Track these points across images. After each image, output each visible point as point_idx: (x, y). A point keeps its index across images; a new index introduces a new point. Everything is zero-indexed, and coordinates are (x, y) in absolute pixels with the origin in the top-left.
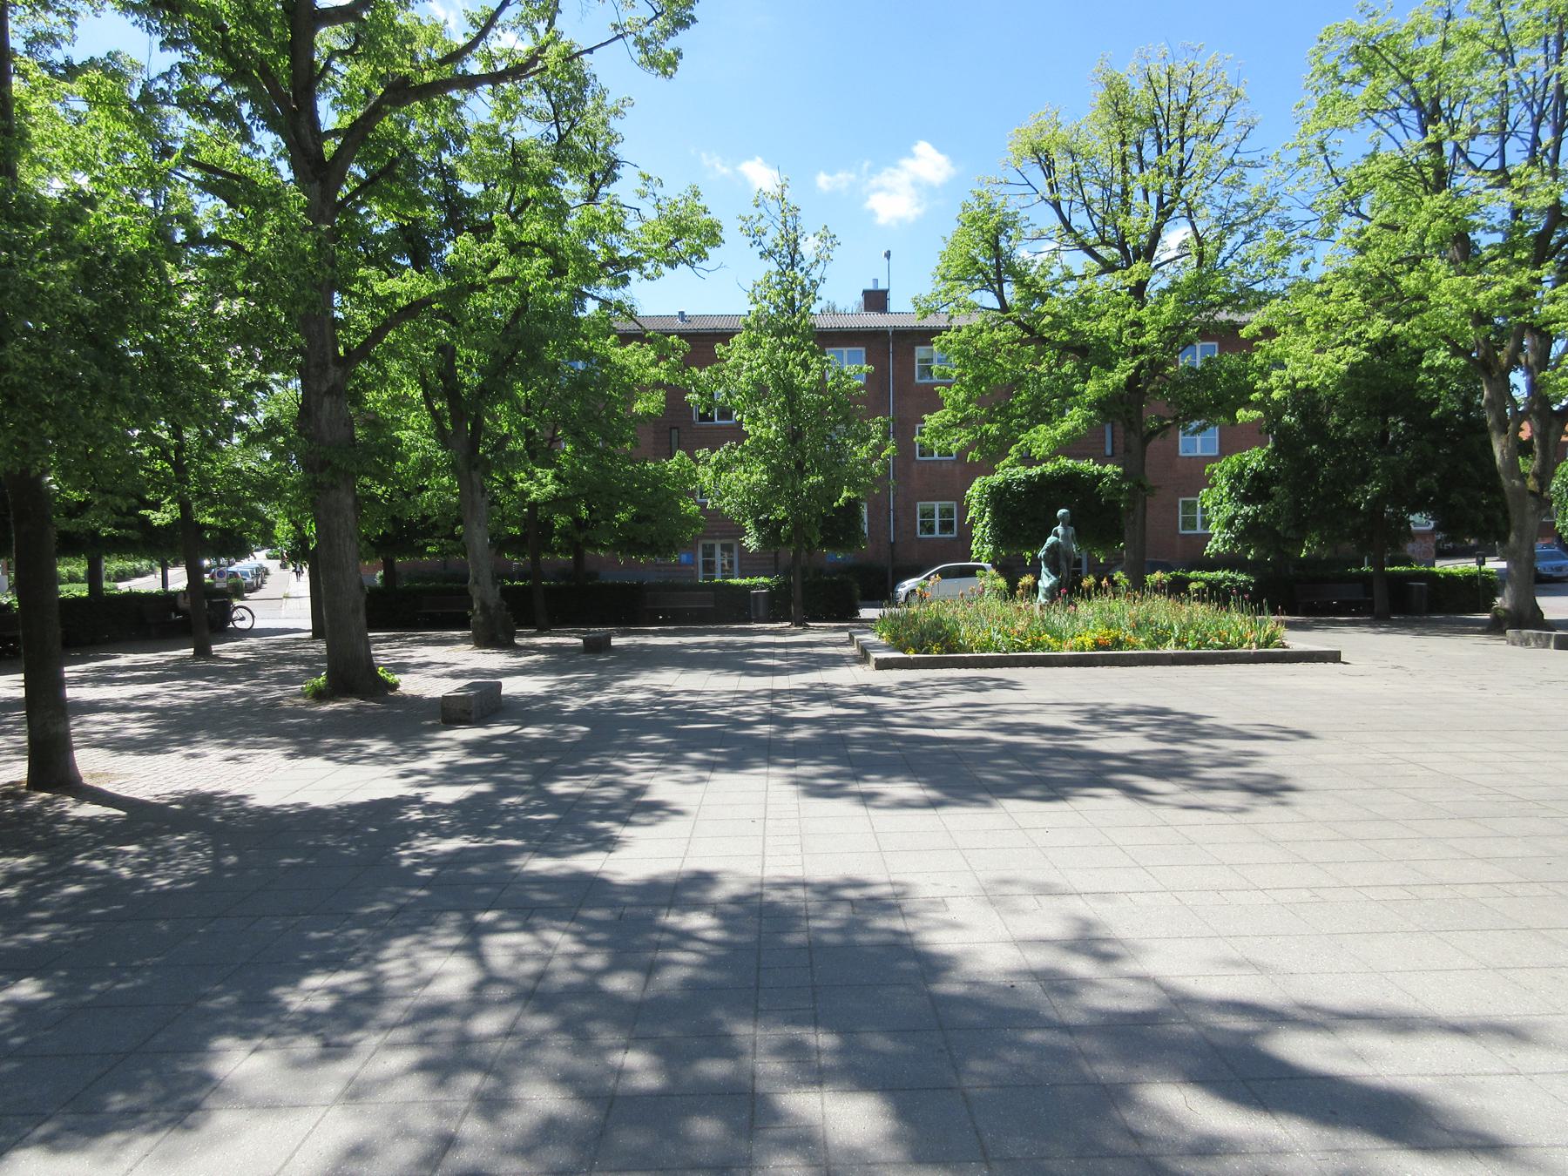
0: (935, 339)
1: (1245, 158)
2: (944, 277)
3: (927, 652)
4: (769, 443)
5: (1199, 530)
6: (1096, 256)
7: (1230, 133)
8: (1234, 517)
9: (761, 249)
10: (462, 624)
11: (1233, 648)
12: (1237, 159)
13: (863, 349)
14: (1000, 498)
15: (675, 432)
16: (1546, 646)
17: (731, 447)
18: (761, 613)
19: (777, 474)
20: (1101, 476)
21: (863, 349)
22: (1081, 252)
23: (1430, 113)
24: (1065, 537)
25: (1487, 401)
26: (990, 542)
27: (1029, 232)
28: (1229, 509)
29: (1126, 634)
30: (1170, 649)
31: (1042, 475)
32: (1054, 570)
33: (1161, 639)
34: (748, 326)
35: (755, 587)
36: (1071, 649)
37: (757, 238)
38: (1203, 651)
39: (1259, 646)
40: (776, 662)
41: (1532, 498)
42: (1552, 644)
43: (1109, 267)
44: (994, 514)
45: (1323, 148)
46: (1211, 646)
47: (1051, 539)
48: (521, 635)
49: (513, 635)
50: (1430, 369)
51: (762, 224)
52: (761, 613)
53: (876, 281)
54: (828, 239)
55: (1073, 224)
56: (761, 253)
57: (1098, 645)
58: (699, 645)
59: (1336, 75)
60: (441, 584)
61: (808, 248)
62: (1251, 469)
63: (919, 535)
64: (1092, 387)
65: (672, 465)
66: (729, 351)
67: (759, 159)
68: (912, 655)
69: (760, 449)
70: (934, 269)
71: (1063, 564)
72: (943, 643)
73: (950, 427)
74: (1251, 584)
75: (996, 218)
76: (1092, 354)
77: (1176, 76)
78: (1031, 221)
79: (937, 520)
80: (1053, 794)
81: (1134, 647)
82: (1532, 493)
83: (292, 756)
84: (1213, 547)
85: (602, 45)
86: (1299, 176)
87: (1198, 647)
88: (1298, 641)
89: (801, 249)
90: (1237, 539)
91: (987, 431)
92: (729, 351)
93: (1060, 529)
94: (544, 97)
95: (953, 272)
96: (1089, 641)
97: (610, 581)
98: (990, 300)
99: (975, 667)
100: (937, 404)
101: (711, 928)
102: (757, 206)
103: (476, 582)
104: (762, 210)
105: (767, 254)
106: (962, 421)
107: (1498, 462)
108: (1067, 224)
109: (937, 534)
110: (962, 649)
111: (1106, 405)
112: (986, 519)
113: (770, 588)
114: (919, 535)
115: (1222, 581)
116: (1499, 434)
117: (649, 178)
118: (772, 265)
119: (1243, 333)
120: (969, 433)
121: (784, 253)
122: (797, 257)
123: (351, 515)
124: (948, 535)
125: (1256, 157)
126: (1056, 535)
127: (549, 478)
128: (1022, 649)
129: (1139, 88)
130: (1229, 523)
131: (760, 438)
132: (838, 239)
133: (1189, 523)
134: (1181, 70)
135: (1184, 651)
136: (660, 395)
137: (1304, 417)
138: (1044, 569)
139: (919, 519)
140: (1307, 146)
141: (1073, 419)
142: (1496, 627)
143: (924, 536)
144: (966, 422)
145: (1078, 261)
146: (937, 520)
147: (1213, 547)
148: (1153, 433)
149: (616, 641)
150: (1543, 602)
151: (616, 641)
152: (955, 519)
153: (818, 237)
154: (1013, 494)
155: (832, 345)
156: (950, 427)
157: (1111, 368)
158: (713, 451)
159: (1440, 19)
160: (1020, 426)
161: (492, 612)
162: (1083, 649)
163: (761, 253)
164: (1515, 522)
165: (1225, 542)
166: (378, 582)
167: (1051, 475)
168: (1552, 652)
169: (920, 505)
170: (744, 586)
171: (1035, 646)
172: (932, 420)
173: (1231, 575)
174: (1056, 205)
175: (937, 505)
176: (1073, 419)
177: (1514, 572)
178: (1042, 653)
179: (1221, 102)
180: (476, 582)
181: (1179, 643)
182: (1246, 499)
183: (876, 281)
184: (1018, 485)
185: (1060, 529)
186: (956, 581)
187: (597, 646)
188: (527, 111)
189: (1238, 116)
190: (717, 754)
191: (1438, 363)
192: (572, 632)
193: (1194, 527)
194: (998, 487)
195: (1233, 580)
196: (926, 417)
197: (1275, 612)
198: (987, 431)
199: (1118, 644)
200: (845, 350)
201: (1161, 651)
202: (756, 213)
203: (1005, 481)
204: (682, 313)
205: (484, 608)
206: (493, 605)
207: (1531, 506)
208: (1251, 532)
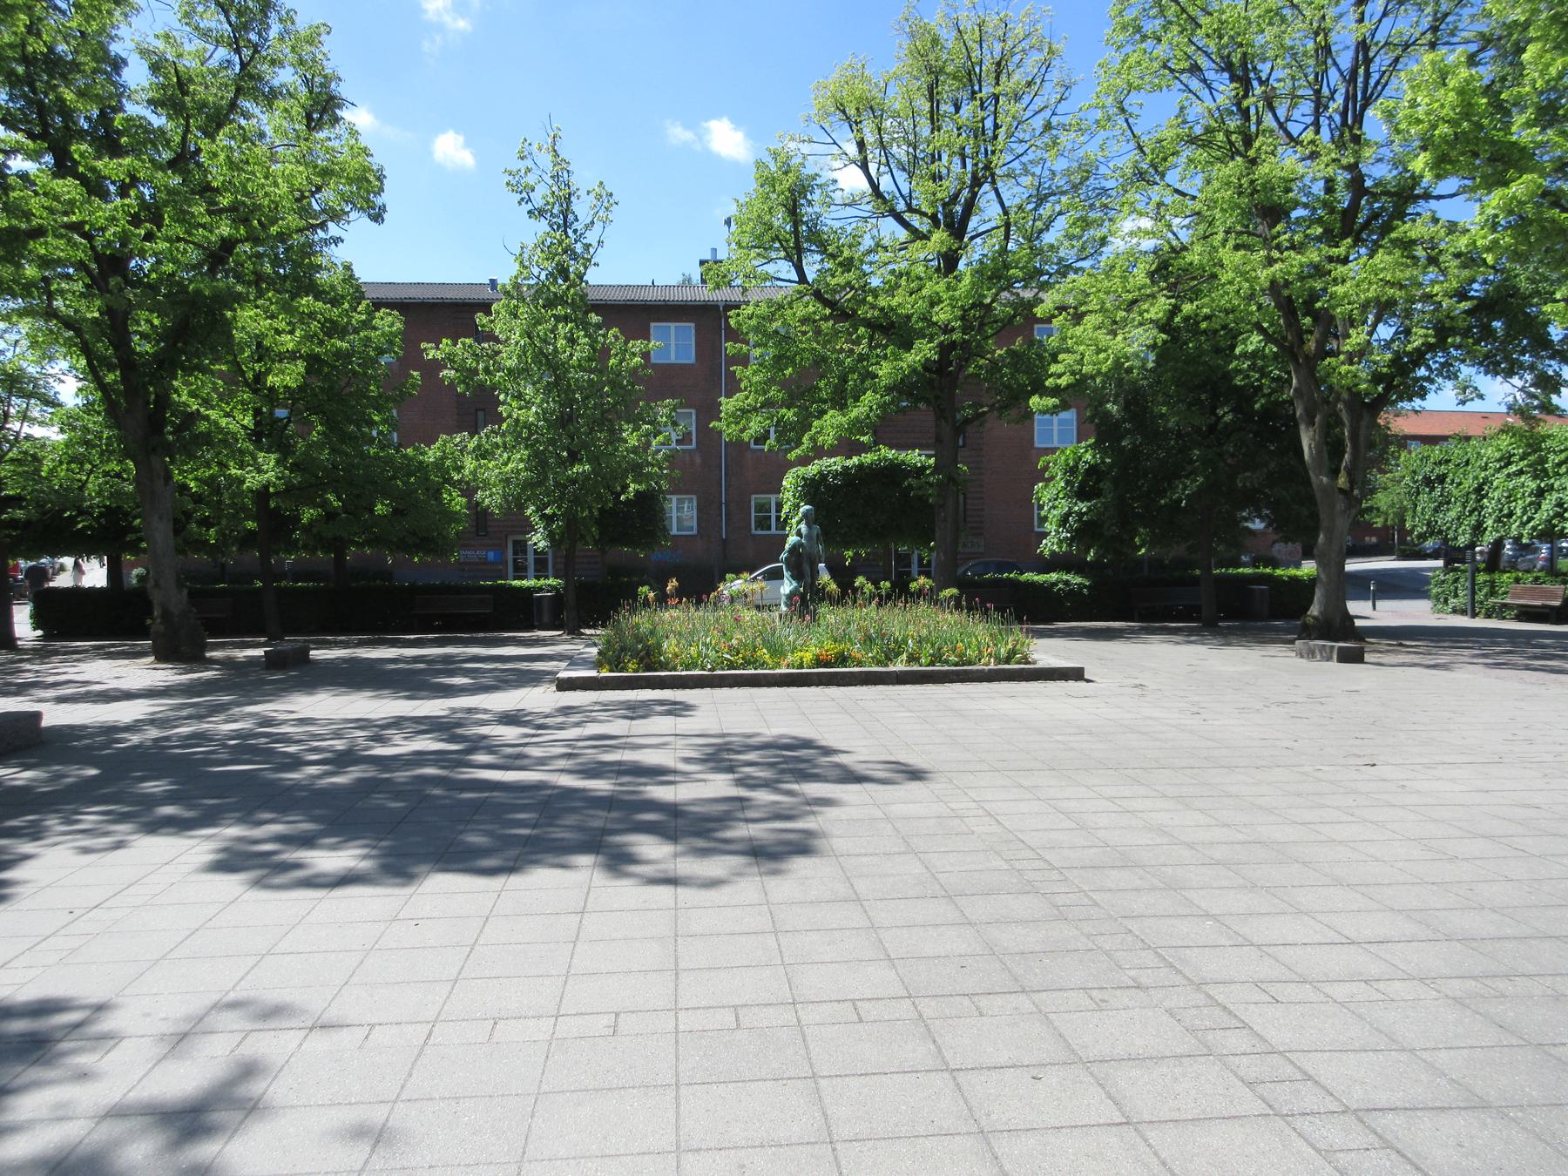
1: (1063, 120)
2: (739, 244)
5: (773, 530)
6: (906, 225)
7: (1049, 94)
8: (1069, 514)
9: (529, 206)
10: (140, 632)
11: (970, 663)
12: (1054, 121)
13: (693, 325)
14: (813, 490)
15: (481, 414)
16: (1329, 659)
18: (546, 618)
19: (539, 461)
21: (693, 325)
22: (891, 218)
23: (1241, 73)
24: (809, 537)
25: (1295, 390)
28: (1064, 506)
29: (856, 650)
30: (899, 666)
31: (860, 467)
33: (890, 656)
34: (507, 293)
35: (540, 589)
36: (788, 666)
37: (524, 195)
41: (1341, 497)
42: (1335, 657)
43: (917, 235)
46: (947, 662)
49: (205, 647)
50: (1244, 355)
51: (531, 179)
52: (546, 618)
53: (714, 251)
54: (605, 199)
56: (529, 212)
57: (819, 662)
58: (416, 659)
59: (1138, 29)
61: (582, 209)
62: (1086, 462)
63: (754, 531)
64: (884, 370)
65: (431, 454)
66: (492, 321)
67: (725, 120)
68: (605, 674)
69: (522, 434)
72: (641, 660)
74: (1085, 587)
75: (791, 178)
76: (895, 331)
81: (860, 664)
82: (1341, 490)
84: (1049, 546)
86: (1098, 140)
87: (932, 663)
89: (574, 207)
90: (1072, 539)
91: (783, 416)
92: (492, 321)
94: (222, 18)
95: (746, 240)
96: (808, 657)
98: (786, 270)
99: (662, 688)
100: (733, 388)
102: (522, 158)
103: (157, 585)
104: (528, 163)
105: (533, 213)
107: (1306, 457)
108: (875, 187)
109: (773, 530)
110: (664, 666)
111: (903, 387)
114: (754, 531)
115: (1055, 584)
116: (1307, 427)
118: (542, 226)
119: (1039, 311)
121: (555, 211)
122: (571, 217)
127: (272, 463)
128: (731, 666)
129: (948, 37)
130: (1064, 521)
132: (615, 198)
133: (763, 523)
134: (992, 22)
135: (916, 668)
136: (301, 366)
137: (1126, 407)
138: (786, 574)
139: (753, 514)
140: (1104, 107)
141: (867, 404)
142: (1307, 632)
144: (768, 404)
147: (1049, 546)
148: (967, 421)
149: (316, 654)
150: (1354, 607)
151: (316, 654)
153: (592, 195)
154: (828, 486)
155: (658, 320)
157: (908, 347)
163: (529, 212)
164: (1325, 523)
165: (1060, 542)
166: (134, 581)
167: (870, 466)
168: (1334, 665)
169: (755, 499)
170: (528, 588)
171: (747, 663)
172: (728, 405)
173: (1065, 577)
174: (864, 167)
177: (1323, 576)
178: (753, 671)
179: (1036, 57)
180: (157, 585)
181: (913, 658)
183: (714, 251)
189: (1054, 75)
191: (1251, 348)
193: (769, 528)
194: (812, 480)
195: (1067, 583)
197: (1021, 622)
198: (783, 416)
200: (673, 325)
201: (891, 668)
202: (522, 165)
203: (820, 472)
205: (166, 615)
207: (1340, 505)
208: (1085, 532)
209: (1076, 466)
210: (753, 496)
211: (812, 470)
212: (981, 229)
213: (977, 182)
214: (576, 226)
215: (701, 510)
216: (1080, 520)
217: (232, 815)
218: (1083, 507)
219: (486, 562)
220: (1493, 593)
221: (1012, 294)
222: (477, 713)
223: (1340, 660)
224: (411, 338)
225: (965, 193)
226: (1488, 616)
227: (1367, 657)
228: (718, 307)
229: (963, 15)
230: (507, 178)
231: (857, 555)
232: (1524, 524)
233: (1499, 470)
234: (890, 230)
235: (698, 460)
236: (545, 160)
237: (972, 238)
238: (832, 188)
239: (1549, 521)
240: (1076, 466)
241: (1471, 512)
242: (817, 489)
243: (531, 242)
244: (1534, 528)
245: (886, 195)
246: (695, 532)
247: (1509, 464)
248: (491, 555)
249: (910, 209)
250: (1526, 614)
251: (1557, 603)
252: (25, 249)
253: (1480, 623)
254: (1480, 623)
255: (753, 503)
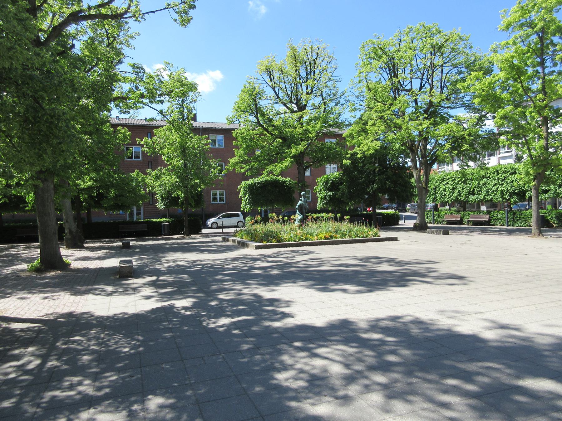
0: (233, 132)
3: (271, 242)
4: (179, 168)
8: (325, 196)
14: (252, 189)
16: (440, 234)
17: (161, 169)
18: (166, 232)
20: (285, 182)
26: (248, 204)
27: (265, 97)
28: (324, 193)
30: (347, 238)
32: (301, 213)
35: (163, 222)
38: (357, 238)
39: (373, 236)
42: (442, 233)
44: (250, 195)
45: (366, 78)
46: (359, 237)
47: (300, 202)
48: (87, 243)
52: (166, 232)
57: (326, 238)
60: (24, 224)
62: (331, 180)
63: (212, 203)
68: (265, 243)
70: (233, 107)
71: (304, 210)
73: (238, 163)
77: (313, 49)
79: (218, 197)
80: (398, 285)
82: (424, 188)
83: (72, 295)
84: (319, 205)
85: (154, 12)
88: (384, 234)
93: (302, 198)
97: (101, 221)
99: (289, 247)
106: (243, 161)
109: (218, 202)
110: (282, 241)
112: (247, 196)
113: (169, 222)
114: (212, 203)
117: (169, 64)
120: (247, 166)
123: (53, 192)
124: (222, 203)
125: (338, 78)
126: (301, 201)
128: (302, 240)
129: (300, 51)
131: (175, 165)
134: (315, 47)
138: (297, 212)
141: (286, 163)
145: (282, 108)
146: (218, 197)
149: (132, 244)
151: (132, 244)
152: (225, 197)
154: (256, 187)
155: (211, 134)
156: (238, 163)
158: (153, 170)
159: (398, 41)
160: (265, 164)
161: (74, 234)
162: (321, 239)
168: (442, 235)
169: (212, 192)
170: (159, 222)
171: (306, 239)
175: (218, 192)
176: (286, 163)
182: (330, 190)
184: (258, 184)
185: (302, 198)
186: (229, 218)
187: (126, 246)
188: (45, 31)
190: (255, 281)
192: (98, 241)
196: (230, 159)
199: (331, 237)
204: (146, 118)
205: (71, 232)
206: (74, 231)
209: (328, 181)
210: (310, 190)
211: (251, 181)
216: (330, 197)
218: (331, 193)
220: (439, 217)
221: (327, 129)
223: (443, 234)
224: (133, 137)
226: (438, 224)
227: (449, 233)
228: (200, 129)
229: (307, 45)
232: (449, 198)
233: (440, 183)
239: (457, 197)
240: (328, 181)
241: (432, 195)
242: (253, 188)
244: (452, 199)
247: (444, 181)
250: (449, 222)
251: (459, 219)
252: (513, 125)
253: (436, 225)
254: (436, 225)
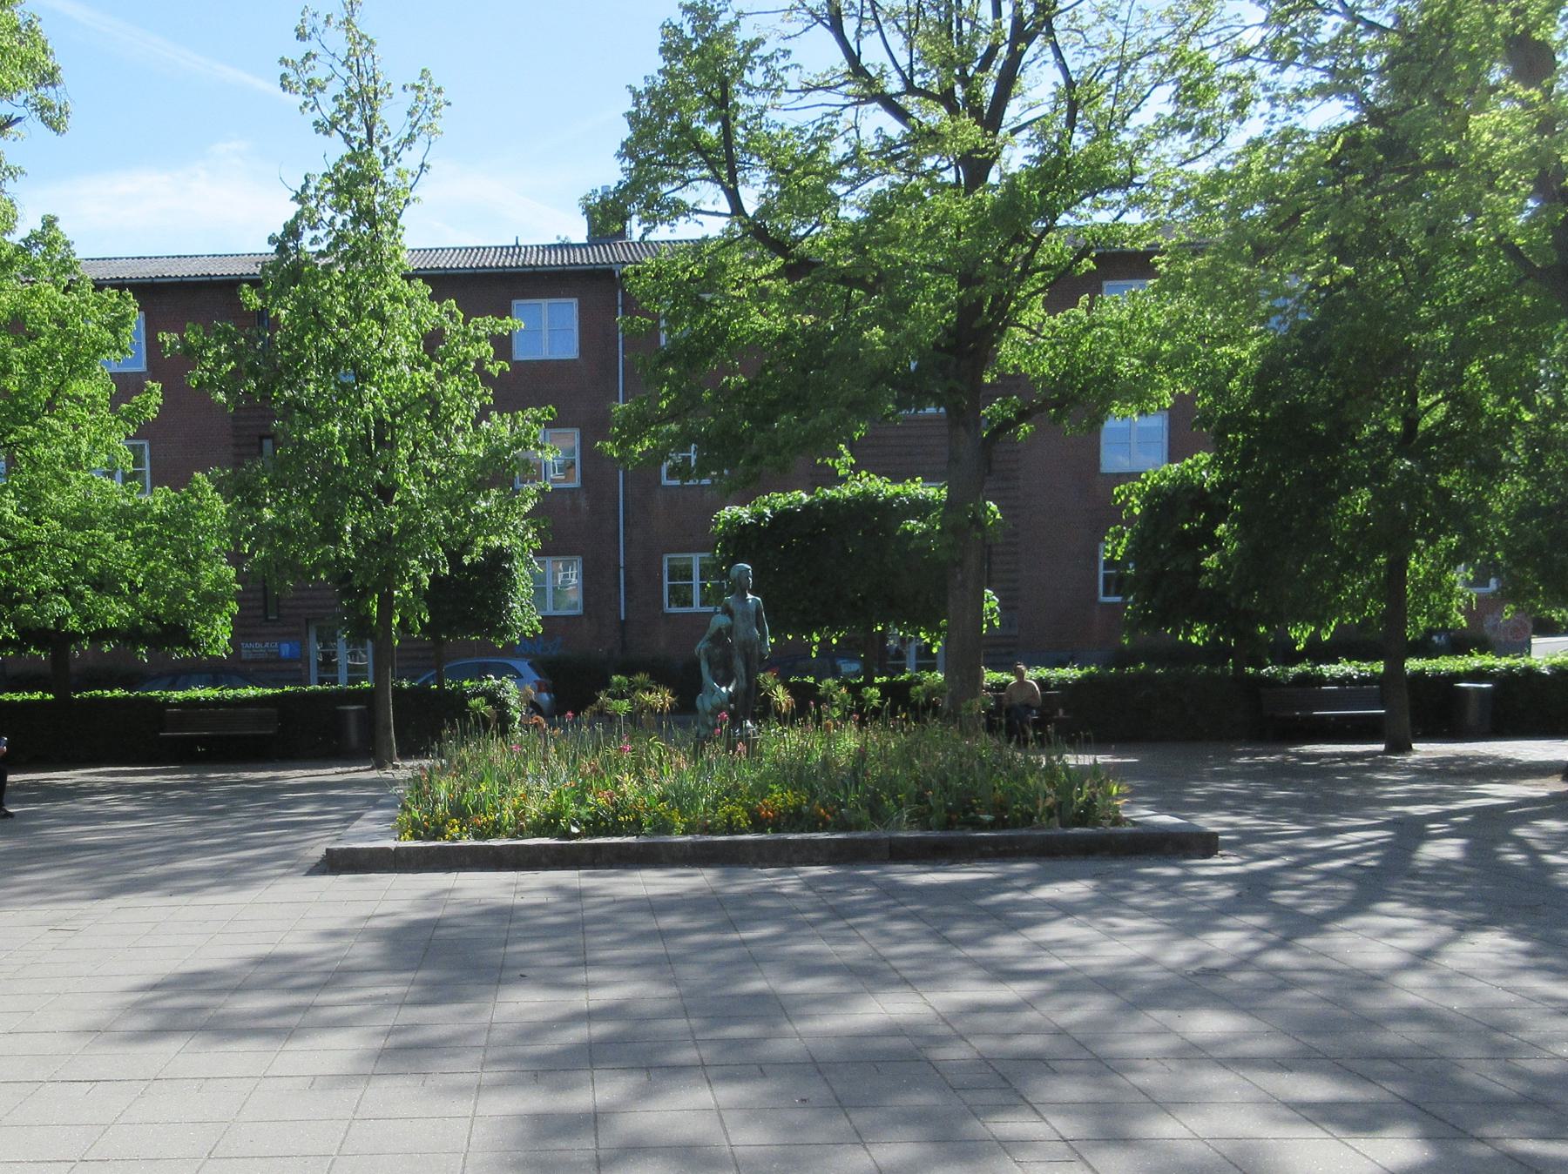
6: (901, 114)
9: (317, 115)
13: (575, 301)
21: (575, 301)
40: (198, 842)
55: (863, 61)
56: (316, 123)
61: (392, 116)
63: (667, 609)
78: (793, 59)
101: (1251, 1036)
104: (312, 46)
105: (326, 127)
108: (853, 58)
139: (666, 583)
143: (675, 610)
174: (836, 27)
200: (545, 302)
212: (1024, 120)
213: (1021, 34)
214: (385, 141)
215: (588, 577)
217: (1425, 864)
219: (279, 659)
222: (1167, 908)
225: (1003, 50)
230: (307, 110)
231: (825, 642)
234: (876, 123)
235: (583, 503)
236: (337, 41)
237: (1014, 132)
238: (783, 62)
243: (320, 168)
245: (870, 69)
246: (579, 611)
248: (286, 649)
249: (910, 89)
255: (666, 566)
